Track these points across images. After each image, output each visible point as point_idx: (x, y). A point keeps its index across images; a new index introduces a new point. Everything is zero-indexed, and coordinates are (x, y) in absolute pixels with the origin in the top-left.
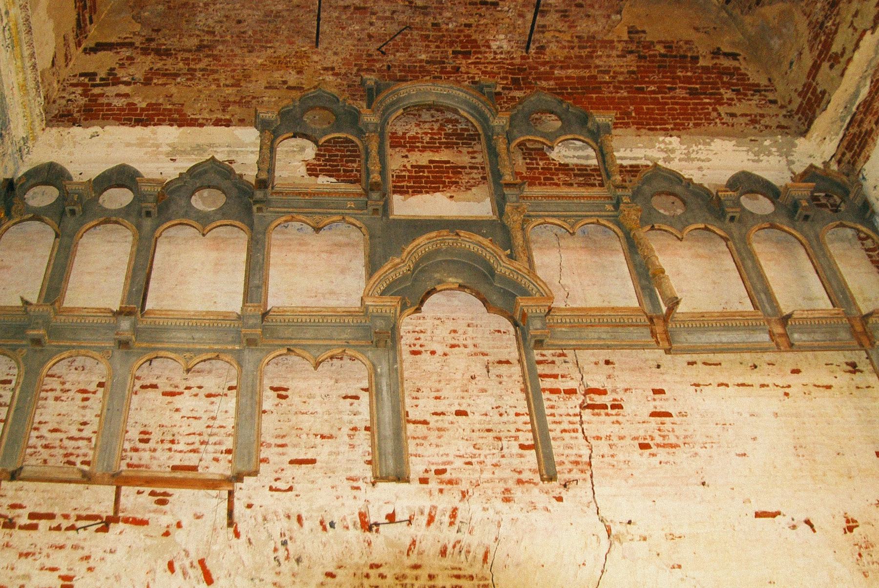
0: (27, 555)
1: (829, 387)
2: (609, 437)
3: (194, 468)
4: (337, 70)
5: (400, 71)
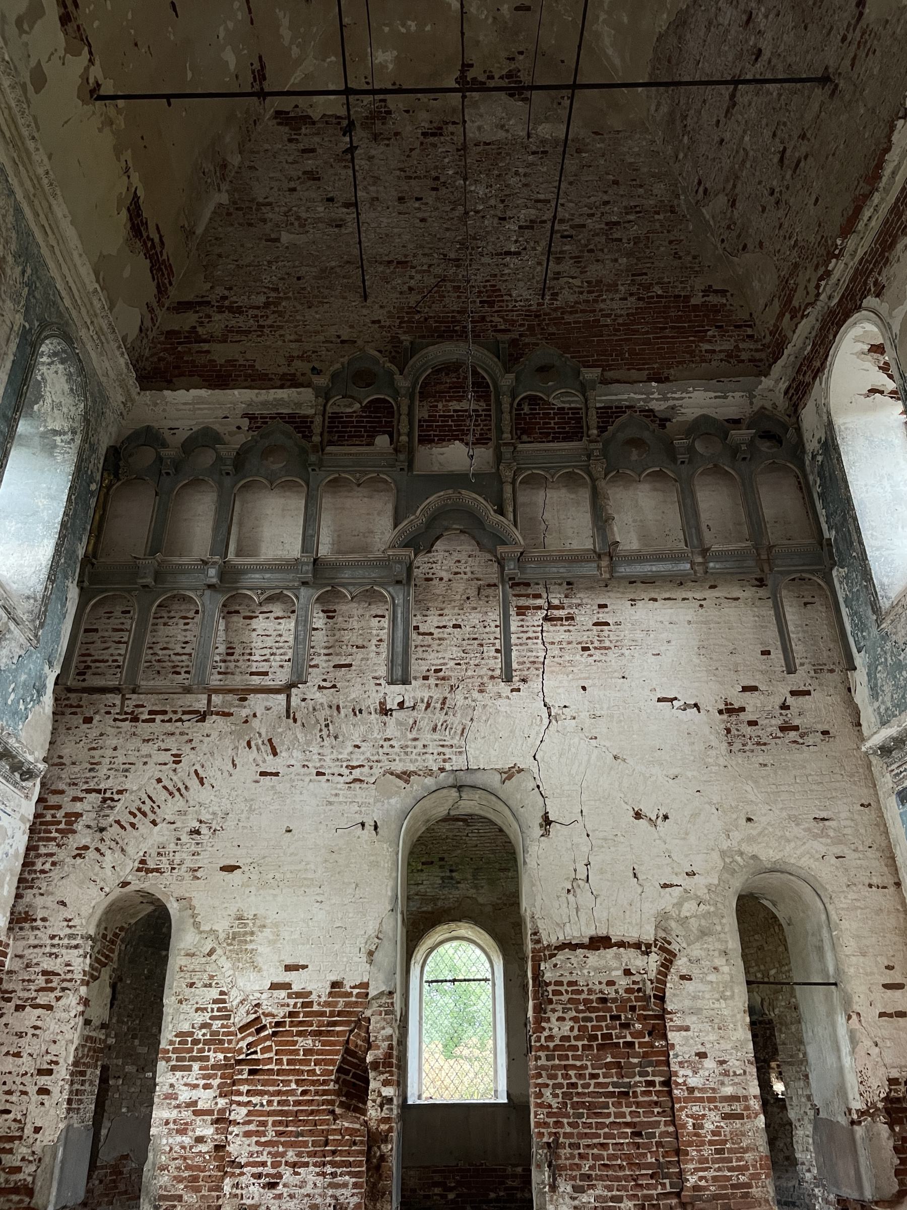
0: (148, 741)
1: (737, 599)
2: (560, 642)
3: (266, 674)
4: (383, 323)
5: (436, 322)
